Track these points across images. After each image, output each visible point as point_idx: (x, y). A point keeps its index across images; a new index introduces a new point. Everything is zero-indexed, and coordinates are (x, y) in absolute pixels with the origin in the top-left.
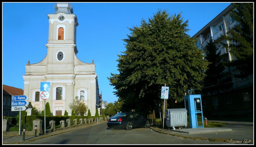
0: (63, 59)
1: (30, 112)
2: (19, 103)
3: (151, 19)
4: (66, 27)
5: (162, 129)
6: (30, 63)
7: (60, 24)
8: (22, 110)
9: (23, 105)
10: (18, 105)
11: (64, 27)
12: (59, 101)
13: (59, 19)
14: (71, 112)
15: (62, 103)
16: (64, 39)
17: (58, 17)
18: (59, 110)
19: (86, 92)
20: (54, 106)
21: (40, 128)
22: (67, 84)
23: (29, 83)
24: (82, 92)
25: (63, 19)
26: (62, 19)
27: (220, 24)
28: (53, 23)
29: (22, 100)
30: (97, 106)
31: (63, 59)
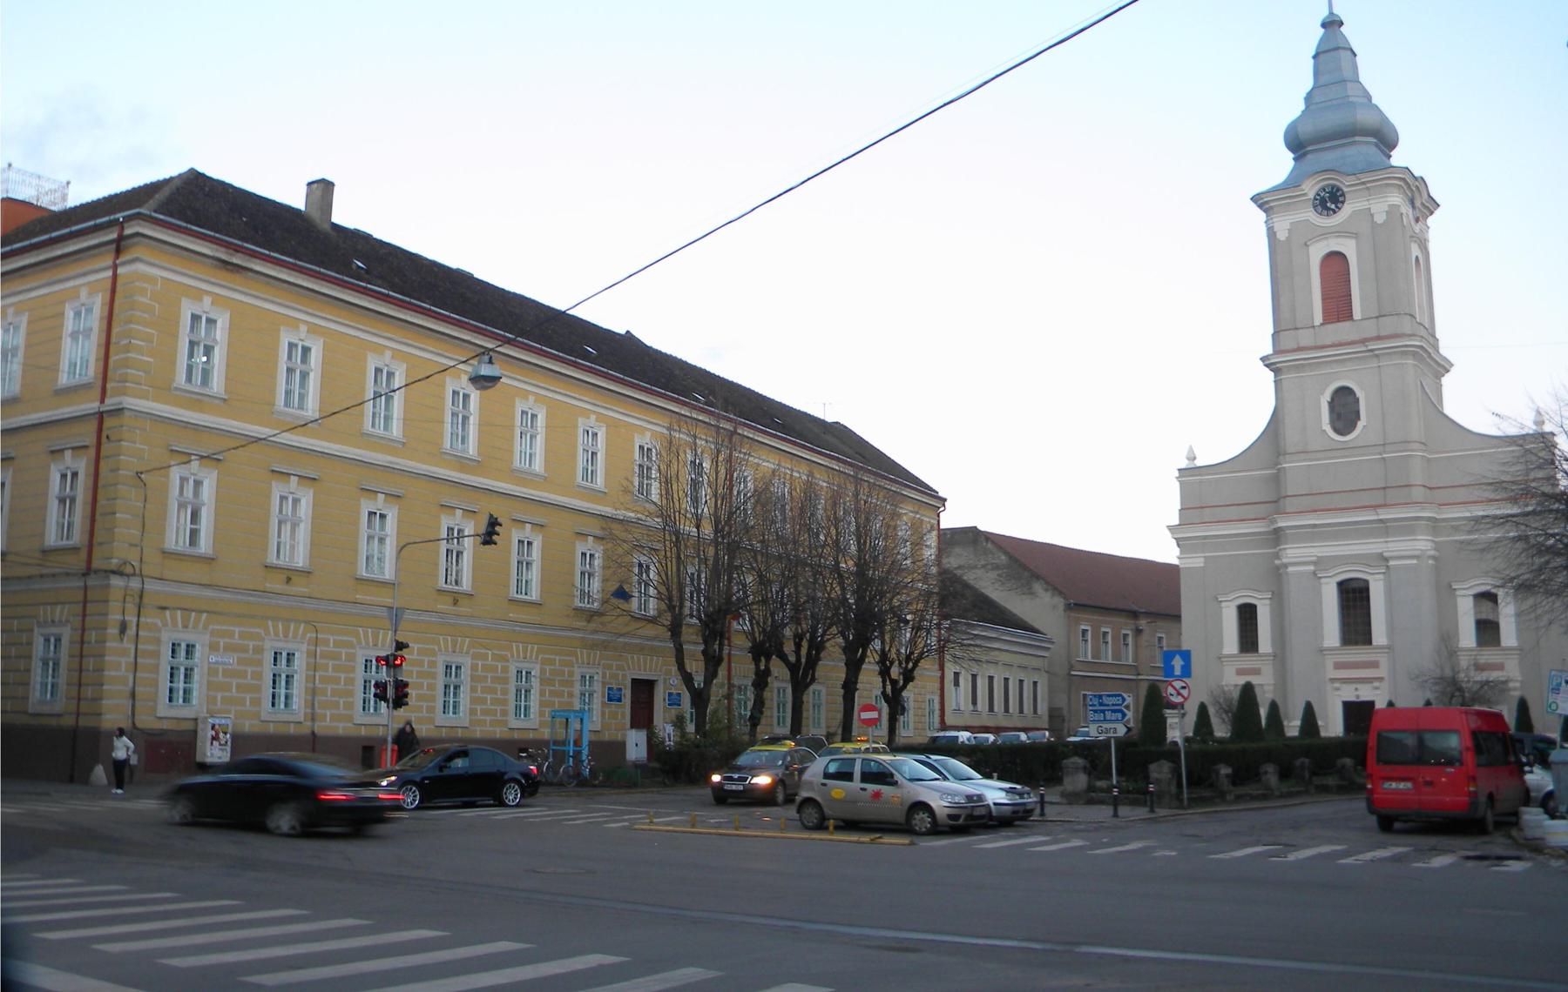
0: (1359, 423)
2: (1108, 714)
3: (1215, 693)
4: (1357, 245)
6: (1195, 458)
7: (1325, 234)
8: (1115, 735)
9: (1118, 720)
10: (1105, 720)
11: (1348, 248)
12: (1357, 654)
13: (1315, 207)
15: (1375, 665)
16: (1357, 314)
18: (1358, 697)
20: (1333, 680)
22: (1392, 563)
23: (1202, 560)
26: (1333, 206)
29: (1113, 705)
30: (1190, 799)
31: (1360, 424)
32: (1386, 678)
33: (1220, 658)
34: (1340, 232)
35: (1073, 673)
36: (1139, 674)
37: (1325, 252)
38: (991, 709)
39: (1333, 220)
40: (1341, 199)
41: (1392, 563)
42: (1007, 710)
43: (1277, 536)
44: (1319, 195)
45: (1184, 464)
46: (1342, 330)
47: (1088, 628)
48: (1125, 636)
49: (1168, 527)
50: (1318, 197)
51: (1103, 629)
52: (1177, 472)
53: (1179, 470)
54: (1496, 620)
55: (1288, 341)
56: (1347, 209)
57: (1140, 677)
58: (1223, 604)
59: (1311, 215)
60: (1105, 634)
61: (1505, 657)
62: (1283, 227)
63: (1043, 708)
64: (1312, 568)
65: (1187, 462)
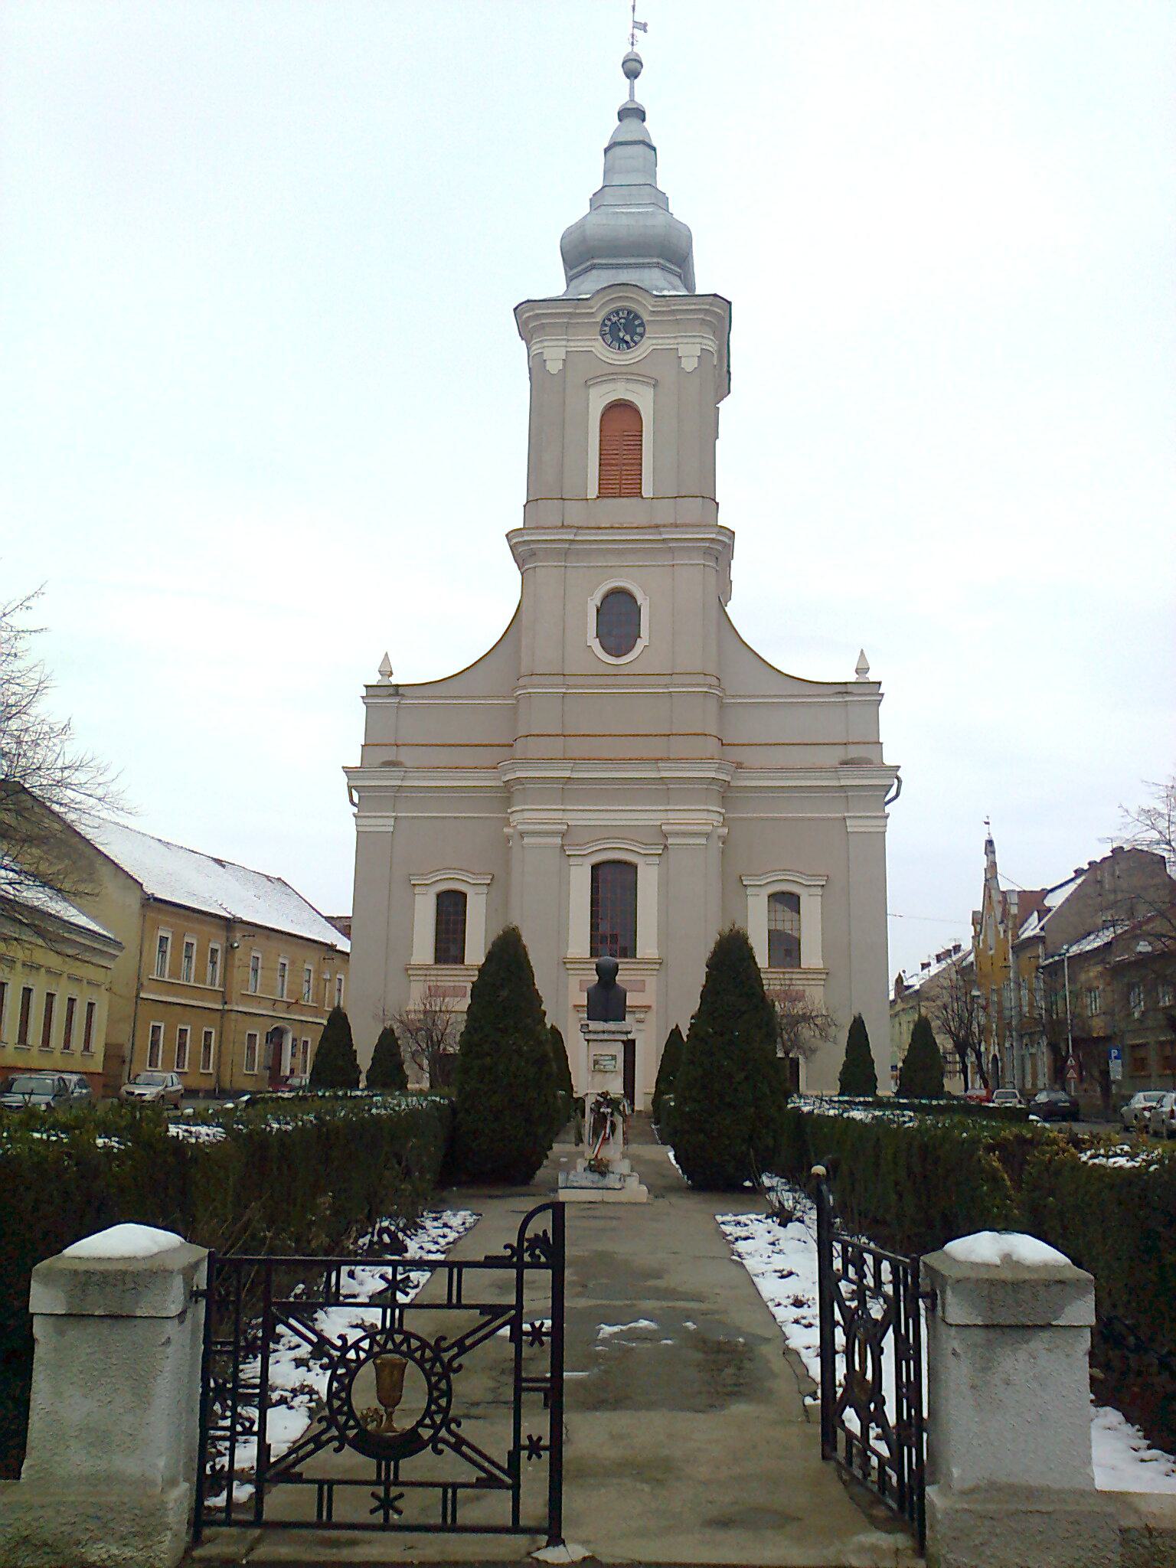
1: (614, 1058)
5: (17, 1041)
7: (613, 375)
11: (643, 399)
14: (34, 1373)
16: (647, 491)
17: (599, 319)
19: (811, 906)
21: (417, 1270)
22: (670, 841)
23: (392, 822)
24: (779, 907)
25: (633, 334)
27: (414, 1302)
28: (563, 371)
31: (640, 644)
32: (654, 1007)
33: (407, 970)
34: (631, 375)
35: (142, 995)
36: (226, 1003)
37: (604, 405)
38: (23, 1038)
39: (637, 353)
40: (639, 330)
41: (526, 840)
42: (46, 1041)
43: (506, 794)
44: (610, 320)
45: (375, 679)
46: (622, 510)
47: (169, 935)
48: (214, 951)
49: (343, 768)
50: (609, 323)
51: (187, 939)
52: (365, 689)
53: (367, 686)
54: (795, 934)
55: (550, 513)
56: (645, 347)
57: (226, 1007)
58: (749, 891)
59: (599, 348)
60: (189, 945)
61: (806, 983)
62: (555, 357)
63: (98, 1046)
64: (558, 841)
65: (379, 677)
